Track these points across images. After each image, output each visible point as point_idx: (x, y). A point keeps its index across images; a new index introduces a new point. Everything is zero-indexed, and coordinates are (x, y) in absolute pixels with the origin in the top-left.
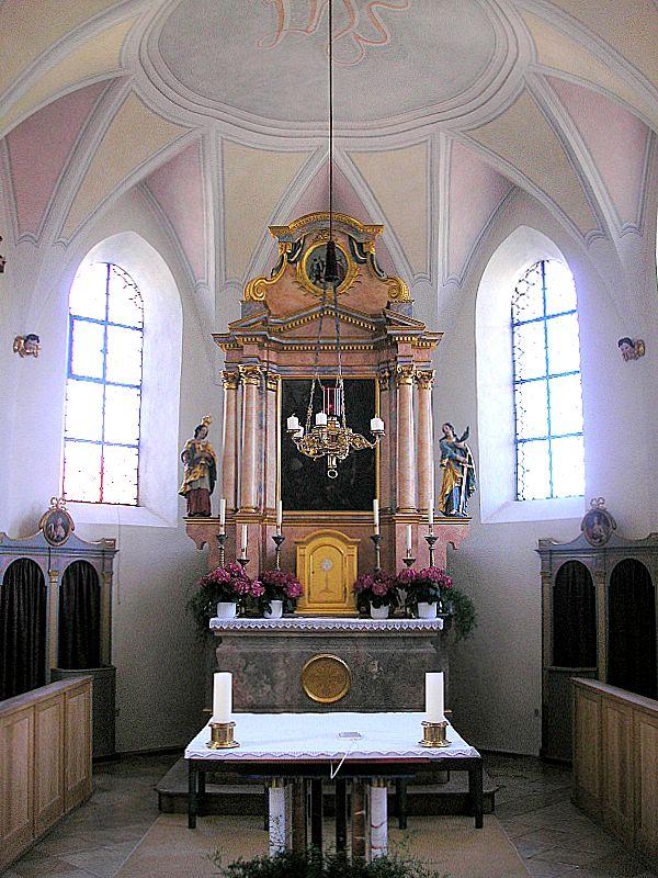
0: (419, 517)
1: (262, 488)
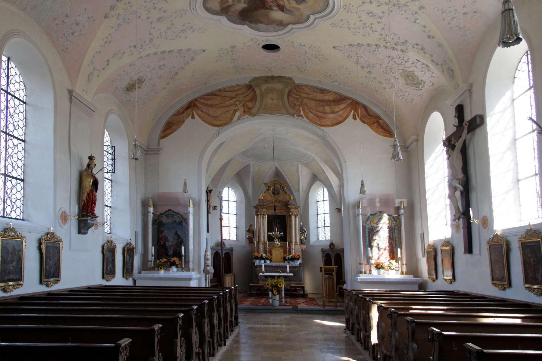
0: (296, 244)
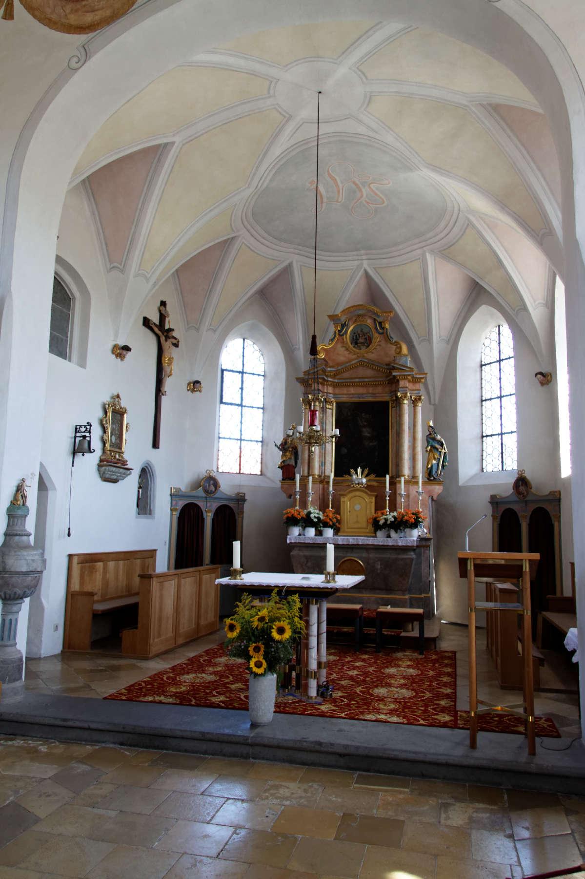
1: (323, 464)
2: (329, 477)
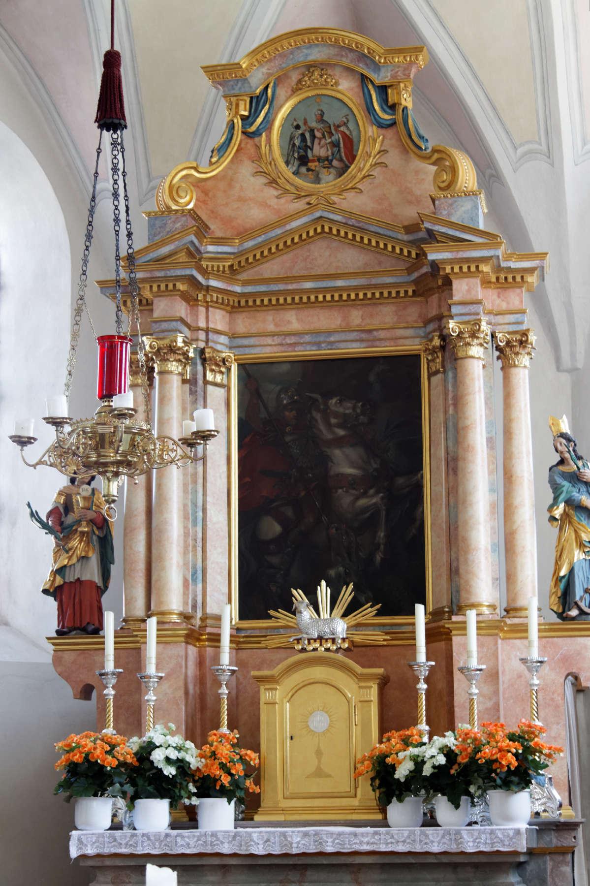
0: (507, 621)
1: (198, 574)
2: (218, 618)
